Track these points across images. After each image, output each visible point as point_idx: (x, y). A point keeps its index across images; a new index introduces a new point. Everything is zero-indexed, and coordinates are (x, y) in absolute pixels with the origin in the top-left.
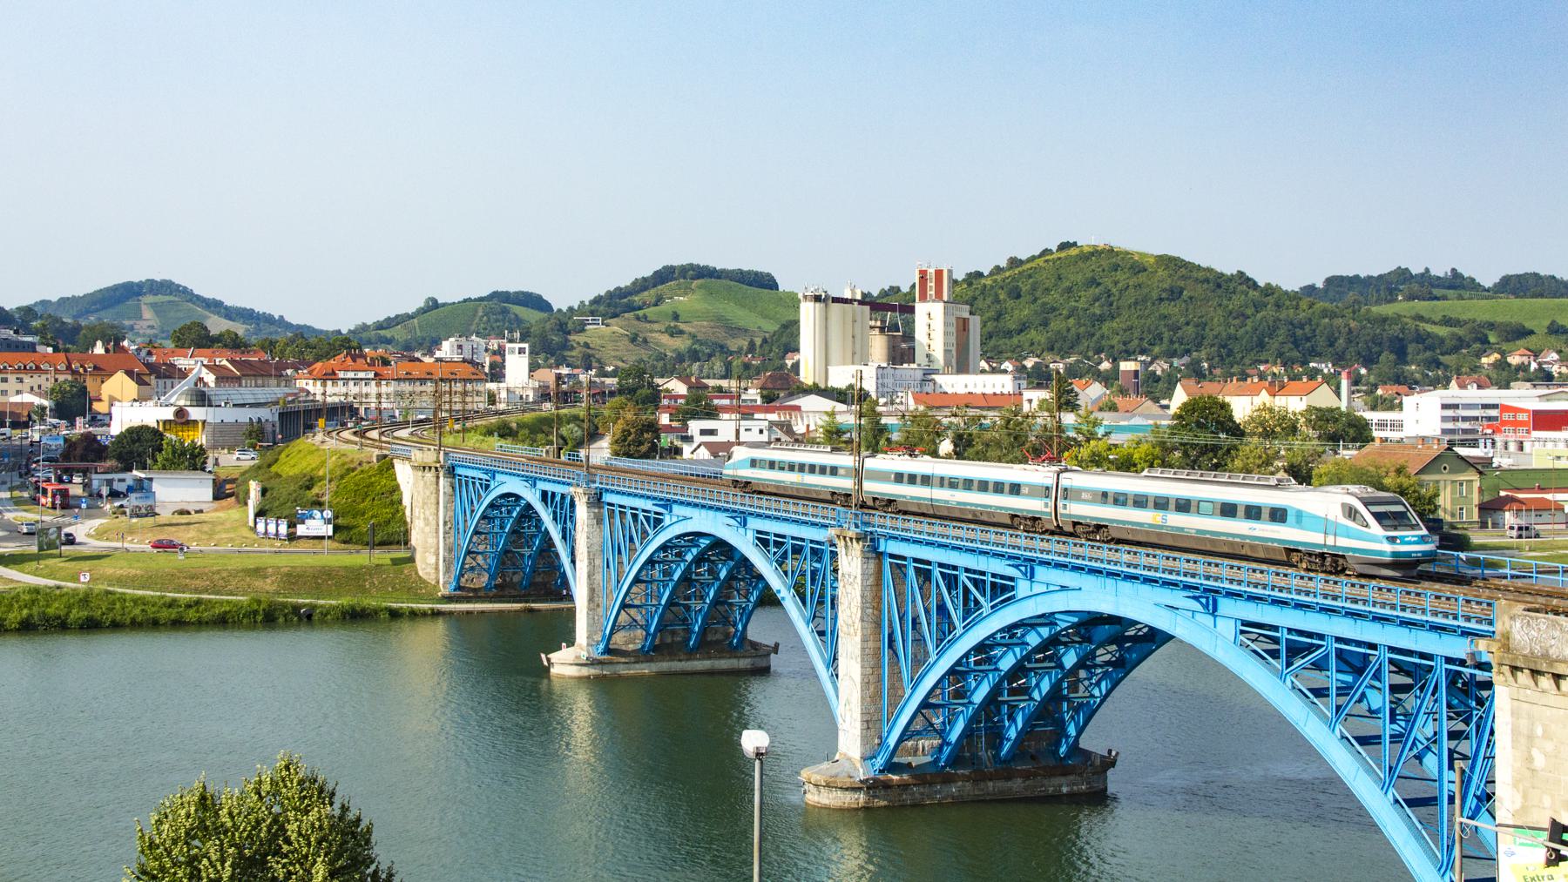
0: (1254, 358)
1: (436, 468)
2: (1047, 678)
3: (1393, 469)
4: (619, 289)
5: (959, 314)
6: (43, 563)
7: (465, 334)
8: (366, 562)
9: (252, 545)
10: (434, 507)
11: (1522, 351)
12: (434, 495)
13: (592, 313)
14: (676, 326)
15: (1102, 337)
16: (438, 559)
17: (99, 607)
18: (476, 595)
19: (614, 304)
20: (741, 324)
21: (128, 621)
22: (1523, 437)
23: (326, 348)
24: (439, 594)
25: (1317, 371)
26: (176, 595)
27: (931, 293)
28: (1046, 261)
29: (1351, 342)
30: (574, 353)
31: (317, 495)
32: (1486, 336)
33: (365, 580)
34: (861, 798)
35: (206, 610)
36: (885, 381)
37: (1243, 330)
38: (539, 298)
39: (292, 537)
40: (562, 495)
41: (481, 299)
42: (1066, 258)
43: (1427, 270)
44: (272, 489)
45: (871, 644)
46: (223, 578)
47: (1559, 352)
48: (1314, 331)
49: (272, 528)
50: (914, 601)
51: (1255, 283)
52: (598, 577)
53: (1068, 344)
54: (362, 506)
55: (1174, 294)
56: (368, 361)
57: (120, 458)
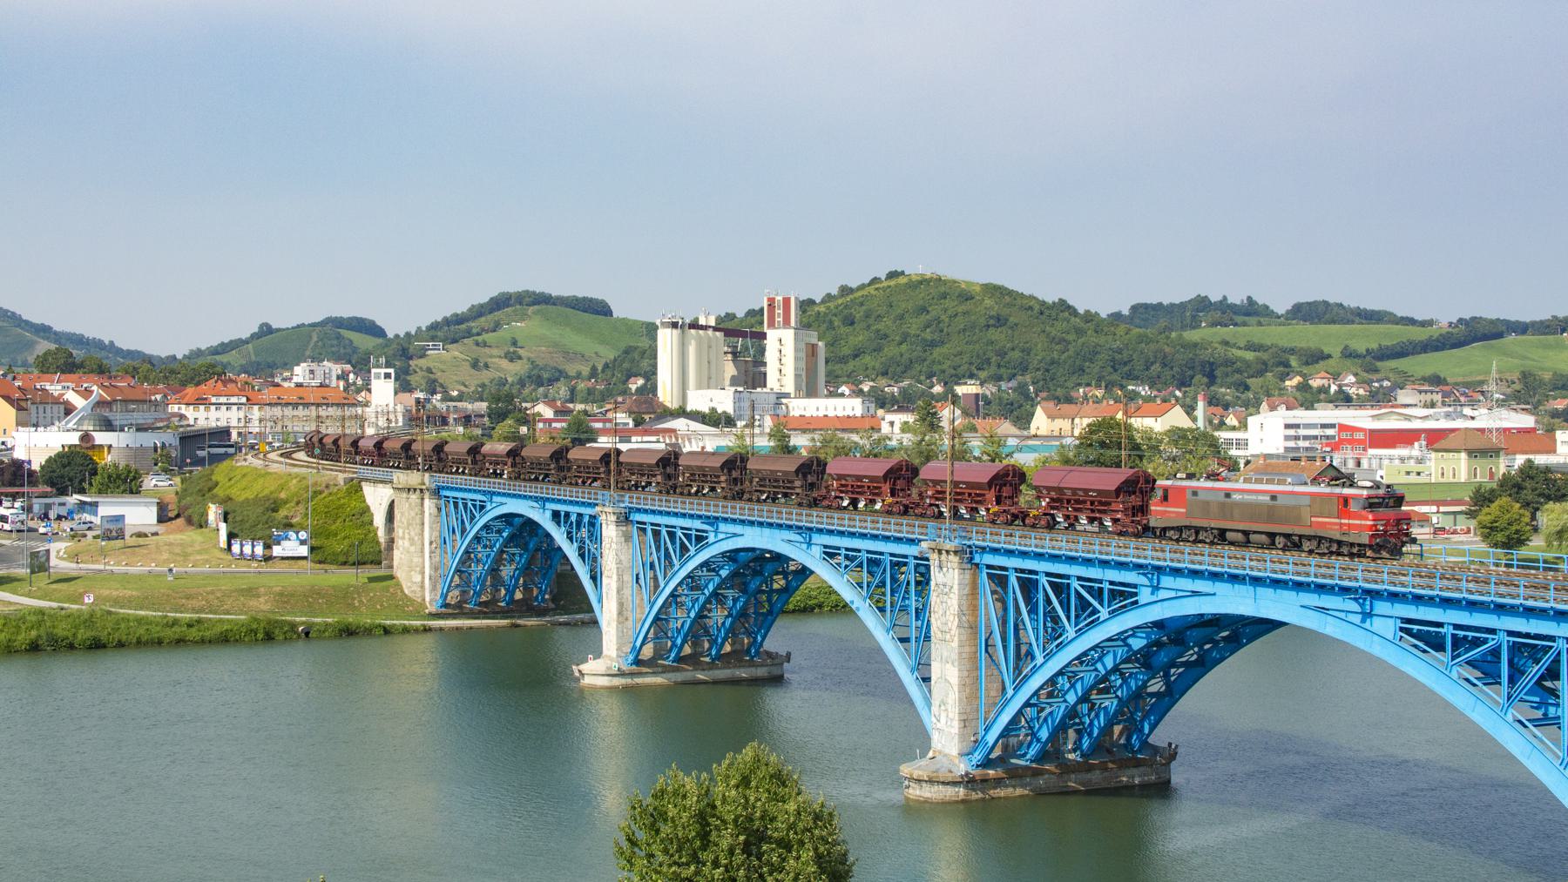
1: (421, 490)
7: (317, 359)
8: (353, 581)
9: (229, 566)
11: (1323, 374)
13: (433, 339)
14: (514, 352)
16: (423, 578)
17: (104, 628)
19: (451, 329)
21: (134, 640)
22: (1360, 454)
24: (427, 611)
25: (1136, 394)
28: (876, 289)
31: (287, 517)
32: (1288, 361)
33: (354, 599)
36: (742, 404)
39: (268, 558)
40: (590, 516)
41: (313, 325)
42: (896, 286)
43: (1225, 298)
44: (234, 511)
47: (1356, 375)
49: (247, 549)
50: (986, 608)
54: (333, 527)
57: (52, 484)
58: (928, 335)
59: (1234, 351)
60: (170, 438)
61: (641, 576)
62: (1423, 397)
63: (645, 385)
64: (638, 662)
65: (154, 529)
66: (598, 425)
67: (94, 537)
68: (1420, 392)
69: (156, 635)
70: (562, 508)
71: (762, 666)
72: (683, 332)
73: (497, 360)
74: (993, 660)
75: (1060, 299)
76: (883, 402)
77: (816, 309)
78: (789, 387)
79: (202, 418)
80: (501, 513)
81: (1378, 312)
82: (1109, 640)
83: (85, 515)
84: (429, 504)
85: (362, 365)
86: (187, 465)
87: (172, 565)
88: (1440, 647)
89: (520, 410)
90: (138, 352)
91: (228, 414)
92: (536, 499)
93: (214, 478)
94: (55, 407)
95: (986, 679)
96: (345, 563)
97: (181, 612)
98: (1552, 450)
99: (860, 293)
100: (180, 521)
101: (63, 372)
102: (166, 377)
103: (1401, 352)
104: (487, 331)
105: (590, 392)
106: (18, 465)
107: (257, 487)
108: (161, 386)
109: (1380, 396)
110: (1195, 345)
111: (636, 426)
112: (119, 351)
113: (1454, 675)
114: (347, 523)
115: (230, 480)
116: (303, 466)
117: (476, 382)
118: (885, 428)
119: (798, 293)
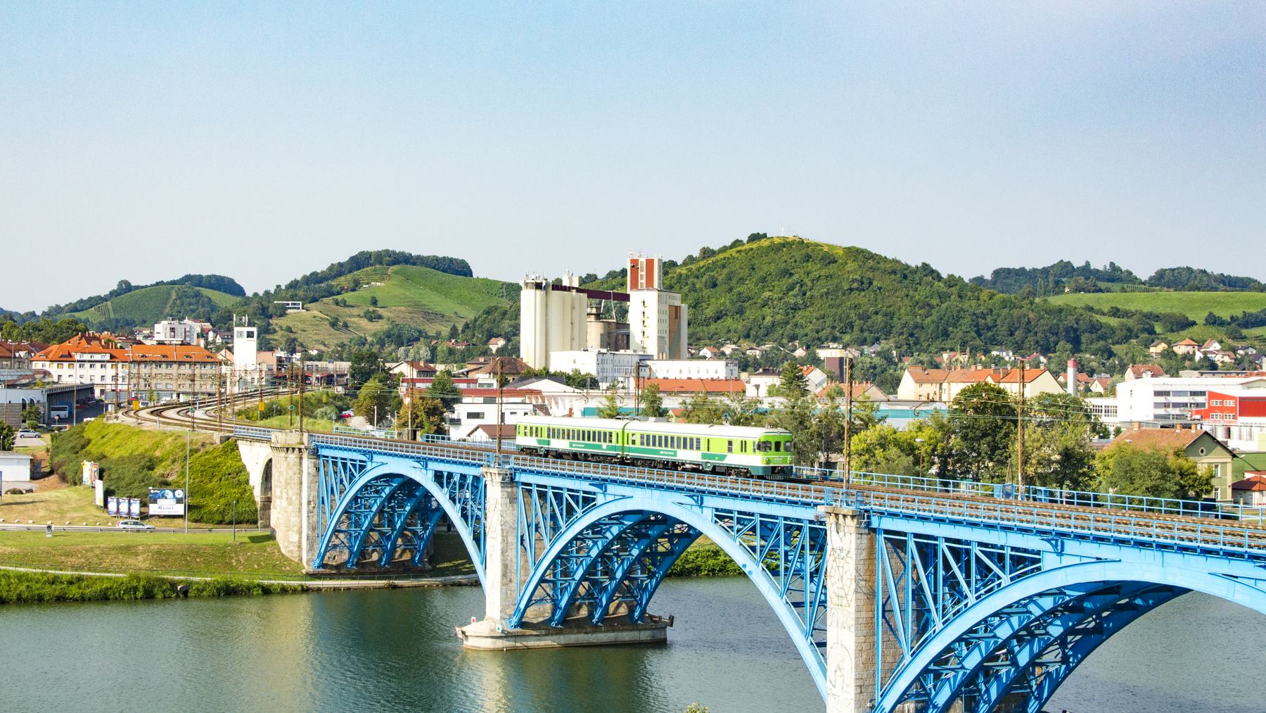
0: (941, 346)
3: (1172, 452)
4: (314, 274)
8: (230, 540)
10: (297, 487)
11: (1188, 341)
12: (297, 476)
13: (292, 298)
16: (300, 538)
18: (339, 571)
20: (438, 309)
21: (15, 597)
22: (1230, 422)
24: (304, 571)
27: (642, 282)
28: (739, 251)
29: (1030, 331)
30: (276, 337)
31: (163, 475)
33: (232, 558)
35: (88, 586)
36: (605, 366)
37: (929, 319)
38: (232, 282)
39: (144, 516)
40: (474, 477)
41: (173, 283)
43: (1088, 264)
44: (110, 469)
45: (864, 614)
46: (97, 556)
47: (1221, 342)
48: (996, 321)
49: (124, 507)
53: (763, 331)
54: (209, 486)
55: (864, 285)
56: (103, 343)
59: (1098, 317)
60: (37, 395)
61: (526, 537)
63: (506, 346)
64: (522, 624)
65: (28, 486)
66: (463, 386)
69: (37, 592)
71: (645, 629)
72: (546, 294)
73: (356, 319)
74: (890, 626)
75: (924, 264)
76: (745, 365)
77: (678, 270)
78: (652, 349)
79: (68, 376)
81: (1242, 279)
82: (1010, 606)
84: (307, 463)
85: (223, 323)
86: (54, 422)
87: (49, 523)
89: (383, 370)
91: (92, 371)
92: (418, 460)
93: (85, 435)
95: (883, 645)
96: (220, 522)
97: (61, 570)
99: (721, 256)
100: (53, 478)
102: (29, 334)
104: (347, 291)
105: (451, 351)
107: (131, 445)
108: (25, 343)
109: (1246, 364)
110: (1061, 310)
114: (223, 482)
115: (103, 437)
116: (176, 424)
117: (335, 342)
118: (751, 393)
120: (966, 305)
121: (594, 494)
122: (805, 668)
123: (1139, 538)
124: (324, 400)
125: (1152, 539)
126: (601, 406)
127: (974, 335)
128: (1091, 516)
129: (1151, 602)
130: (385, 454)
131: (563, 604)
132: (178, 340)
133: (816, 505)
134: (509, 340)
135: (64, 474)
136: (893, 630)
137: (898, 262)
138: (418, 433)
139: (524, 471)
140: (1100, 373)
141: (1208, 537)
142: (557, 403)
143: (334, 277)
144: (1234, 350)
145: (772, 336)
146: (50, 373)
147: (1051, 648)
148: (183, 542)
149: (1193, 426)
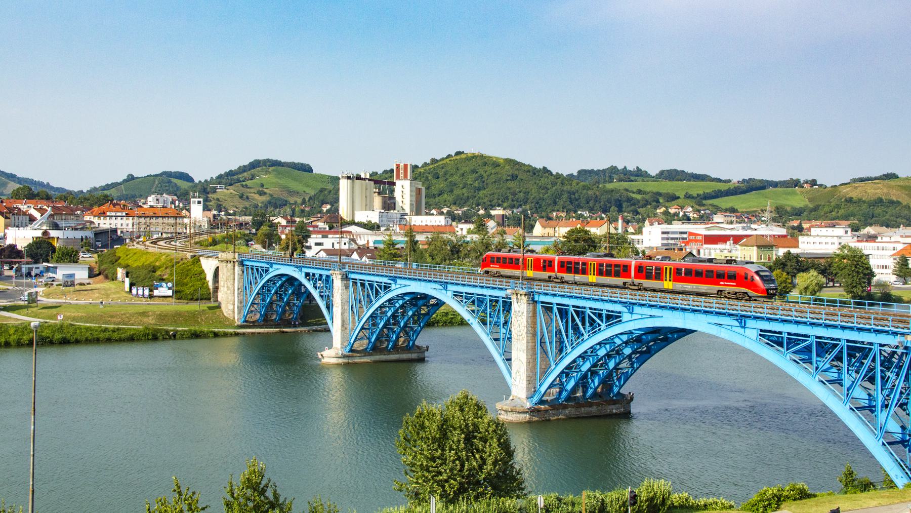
1: (234, 262)
2: (613, 360)
4: (231, 171)
5: (417, 186)
6: (31, 310)
11: (676, 206)
13: (219, 183)
14: (262, 190)
15: (479, 198)
16: (234, 307)
17: (68, 332)
18: (254, 324)
19: (229, 178)
21: (84, 339)
23: (96, 200)
24: (236, 324)
25: (582, 215)
26: (107, 326)
27: (402, 175)
30: (211, 204)
31: (160, 275)
34: (527, 416)
36: (383, 219)
39: (151, 297)
41: (156, 175)
42: (460, 159)
45: (530, 344)
46: (127, 317)
47: (692, 207)
49: (140, 292)
51: (551, 173)
52: (346, 314)
54: (185, 281)
55: (514, 177)
58: (476, 184)
60: (89, 234)
62: (727, 219)
63: (331, 208)
64: (352, 351)
65: (88, 281)
66: (311, 229)
67: (57, 285)
68: (725, 216)
70: (311, 271)
75: (544, 167)
78: (407, 210)
79: (104, 224)
80: (279, 273)
82: (606, 340)
83: (49, 273)
85: (184, 197)
86: (98, 248)
88: (780, 344)
89: (269, 221)
90: (62, 189)
91: (122, 222)
92: (297, 267)
93: (117, 254)
94: (24, 217)
96: (191, 299)
98: (797, 246)
99: (441, 163)
100: (101, 277)
101: (27, 199)
103: (718, 194)
104: (248, 180)
106: (13, 247)
107: (143, 260)
108: (80, 207)
109: (705, 218)
110: (612, 191)
111: (330, 229)
112: (52, 188)
113: (788, 358)
115: (127, 256)
116: (166, 249)
119: (410, 162)
120: (565, 188)
121: (390, 284)
122: (500, 372)
123: (671, 305)
124: (239, 236)
125: (679, 306)
126: (384, 239)
127: (568, 203)
128: (703, 300)
129: (675, 336)
130: (279, 264)
131: (373, 340)
132: (160, 205)
133: (506, 289)
134: (332, 205)
135: (107, 275)
136: (546, 353)
137: (531, 166)
138: (295, 254)
139: (353, 272)
140: (632, 222)
141: (595, 293)
142: (360, 238)
143: (241, 173)
144: (699, 211)
145: (467, 204)
146: (93, 222)
147: (625, 361)
148: (172, 310)
149: (684, 249)
